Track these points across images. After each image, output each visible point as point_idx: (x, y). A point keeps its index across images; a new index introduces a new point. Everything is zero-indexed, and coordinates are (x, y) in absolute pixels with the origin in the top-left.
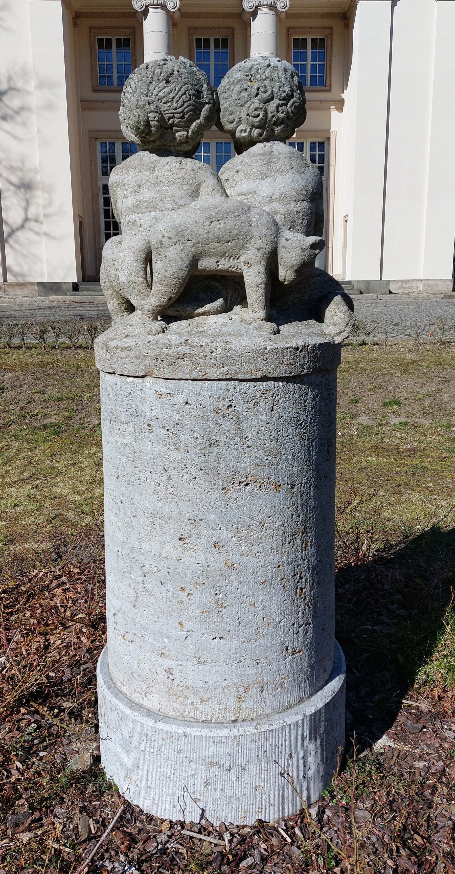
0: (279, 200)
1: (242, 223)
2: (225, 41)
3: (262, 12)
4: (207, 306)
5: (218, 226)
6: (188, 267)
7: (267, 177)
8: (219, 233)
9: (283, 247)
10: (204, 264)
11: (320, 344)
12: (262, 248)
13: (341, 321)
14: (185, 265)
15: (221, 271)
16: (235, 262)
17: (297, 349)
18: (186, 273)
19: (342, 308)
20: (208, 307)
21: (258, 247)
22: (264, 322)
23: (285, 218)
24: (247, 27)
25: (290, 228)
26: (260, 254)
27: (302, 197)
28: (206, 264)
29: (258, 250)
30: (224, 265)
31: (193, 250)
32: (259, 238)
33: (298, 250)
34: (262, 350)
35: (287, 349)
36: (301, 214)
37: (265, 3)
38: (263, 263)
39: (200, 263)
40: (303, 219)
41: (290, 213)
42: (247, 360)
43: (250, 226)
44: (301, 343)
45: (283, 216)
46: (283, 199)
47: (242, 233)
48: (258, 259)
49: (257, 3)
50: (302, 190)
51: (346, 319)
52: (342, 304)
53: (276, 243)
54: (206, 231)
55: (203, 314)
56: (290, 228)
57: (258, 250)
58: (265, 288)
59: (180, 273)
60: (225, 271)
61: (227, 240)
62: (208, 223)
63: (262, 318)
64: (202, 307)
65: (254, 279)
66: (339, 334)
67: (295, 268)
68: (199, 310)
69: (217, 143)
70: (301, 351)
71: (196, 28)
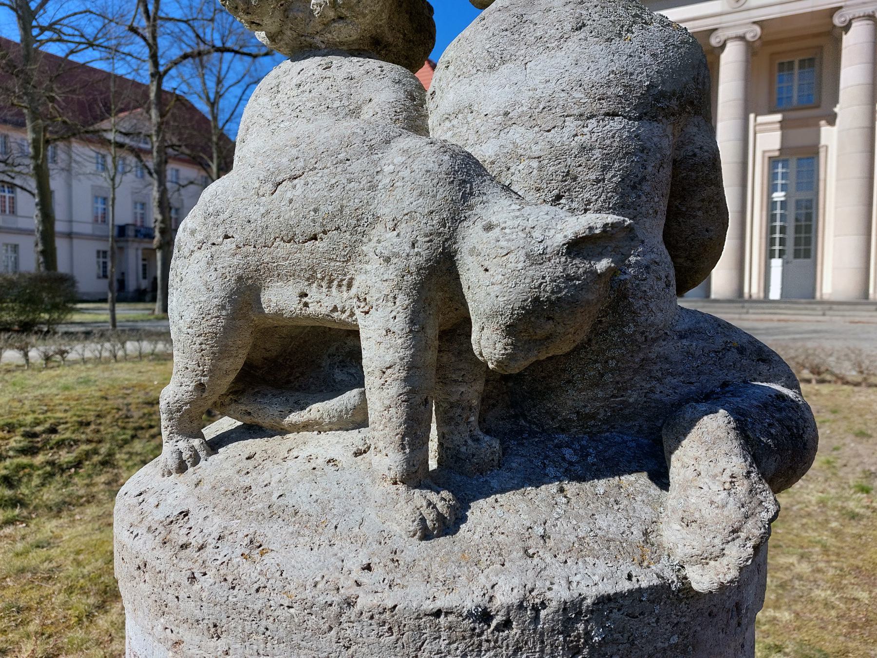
0: (531, 120)
1: (350, 181)
2: (811, 61)
3: (855, 25)
4: (315, 407)
5: (289, 195)
6: (223, 307)
7: (504, 62)
8: (289, 214)
9: (472, 251)
10: (274, 299)
11: (604, 601)
12: (397, 255)
13: (709, 513)
14: (216, 301)
15: (315, 318)
16: (345, 295)
17: (485, 616)
18: (222, 322)
19: (723, 463)
20: (317, 410)
21: (386, 253)
22: (402, 488)
23: (540, 169)
24: (838, 41)
25: (559, 197)
26: (391, 273)
27: (605, 106)
28: (279, 298)
29: (388, 260)
30: (322, 303)
31: (235, 261)
32: (390, 225)
33: (517, 261)
34: (335, 609)
35: (438, 614)
36: (597, 153)
37: (862, 15)
38: (403, 300)
39: (265, 297)
40: (605, 168)
41: (559, 155)
42: (282, 633)
43: (373, 187)
44: (505, 597)
45: (535, 164)
46: (543, 112)
47: (347, 211)
48: (386, 288)
49: (851, 17)
50: (608, 84)
51: (733, 513)
52: (725, 448)
53: (452, 237)
54: (262, 210)
55: (306, 426)
56: (559, 197)
57: (388, 260)
58: (406, 380)
59: (205, 324)
60: (323, 319)
61: (310, 232)
62: (269, 187)
63: (392, 474)
64: (303, 409)
65: (382, 346)
66: (703, 560)
67: (502, 320)
68: (295, 417)
69: (799, 159)
70: (507, 624)
71: (779, 53)
